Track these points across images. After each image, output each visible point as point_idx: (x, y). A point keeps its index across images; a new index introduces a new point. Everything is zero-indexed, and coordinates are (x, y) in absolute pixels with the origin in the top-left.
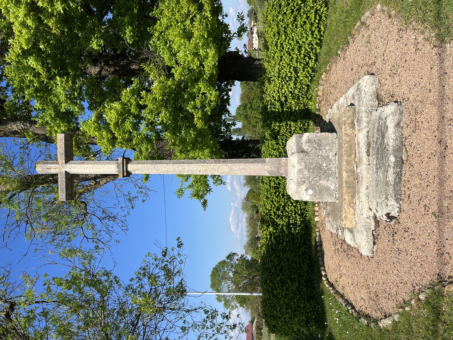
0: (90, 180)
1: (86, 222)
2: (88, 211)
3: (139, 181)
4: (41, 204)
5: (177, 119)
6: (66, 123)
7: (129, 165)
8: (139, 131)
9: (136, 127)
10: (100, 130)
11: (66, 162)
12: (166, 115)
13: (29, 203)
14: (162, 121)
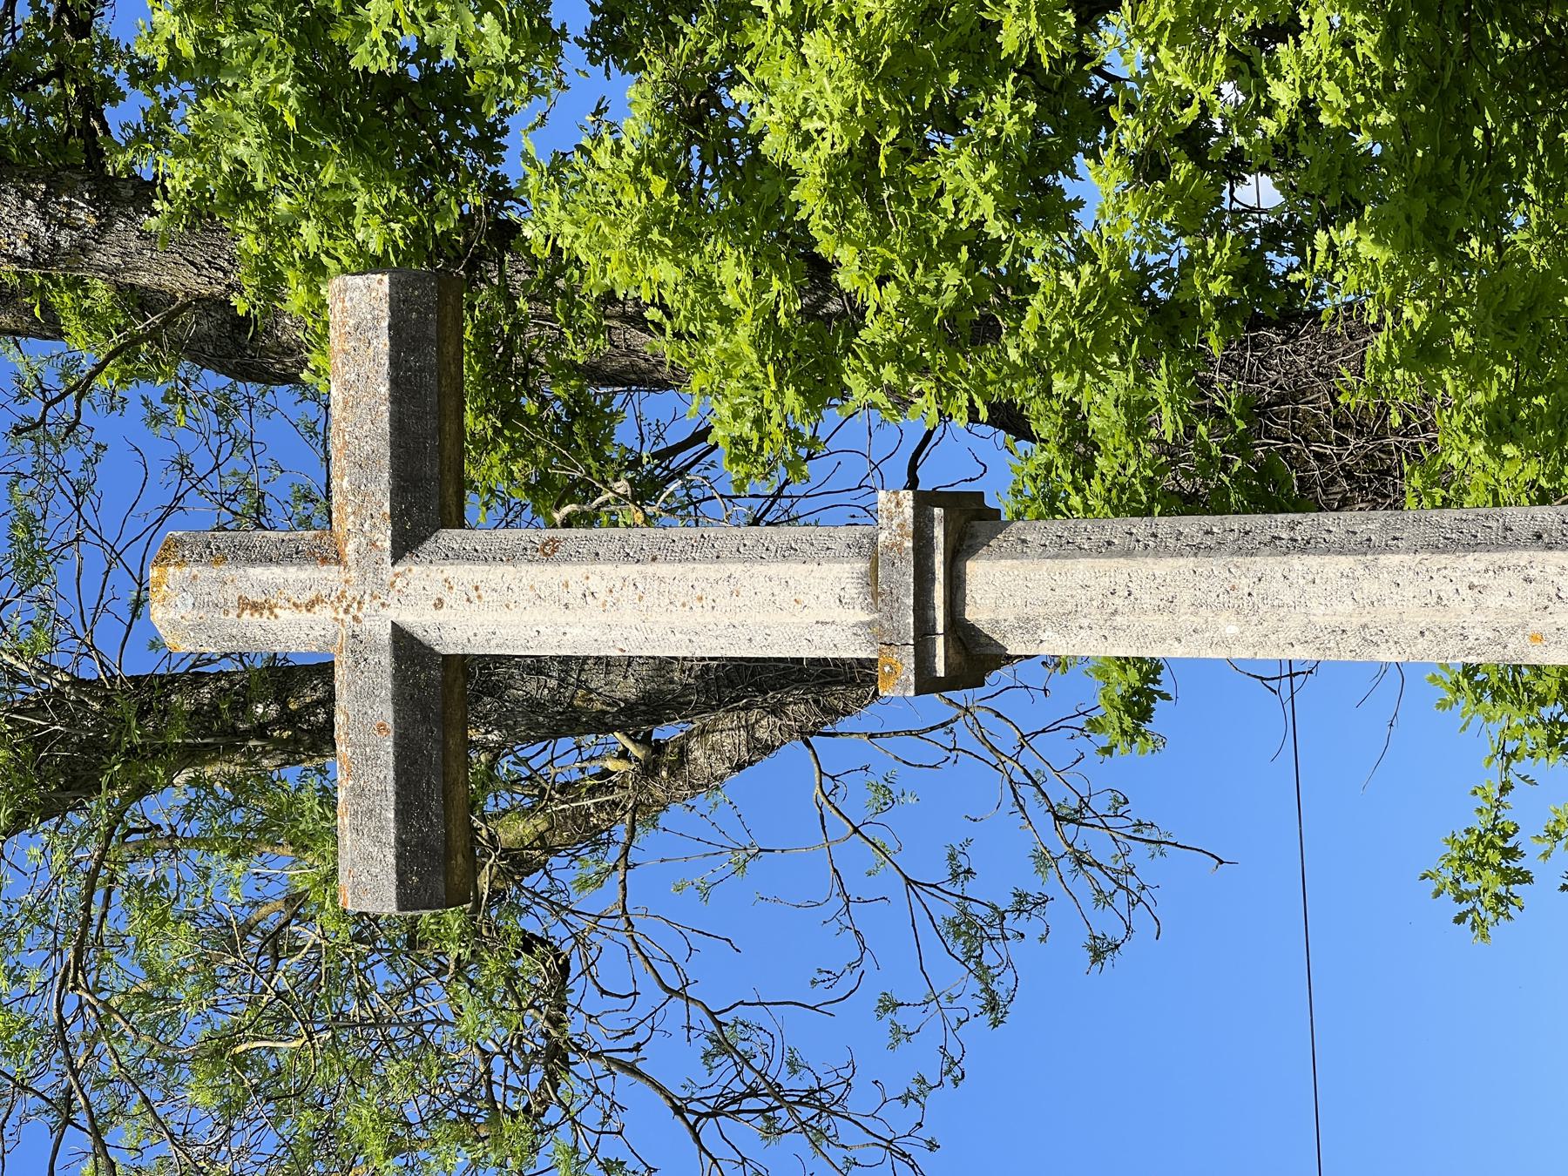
0: (600, 725)
1: (565, 1135)
2: (575, 1025)
3: (1056, 748)
4: (175, 950)
5: (1460, 83)
6: (397, 180)
7: (976, 570)
8: (1070, 225)
9: (1036, 197)
10: (687, 237)
11: (406, 544)
12: (1347, 44)
13: (85, 946)
14: (1308, 108)
